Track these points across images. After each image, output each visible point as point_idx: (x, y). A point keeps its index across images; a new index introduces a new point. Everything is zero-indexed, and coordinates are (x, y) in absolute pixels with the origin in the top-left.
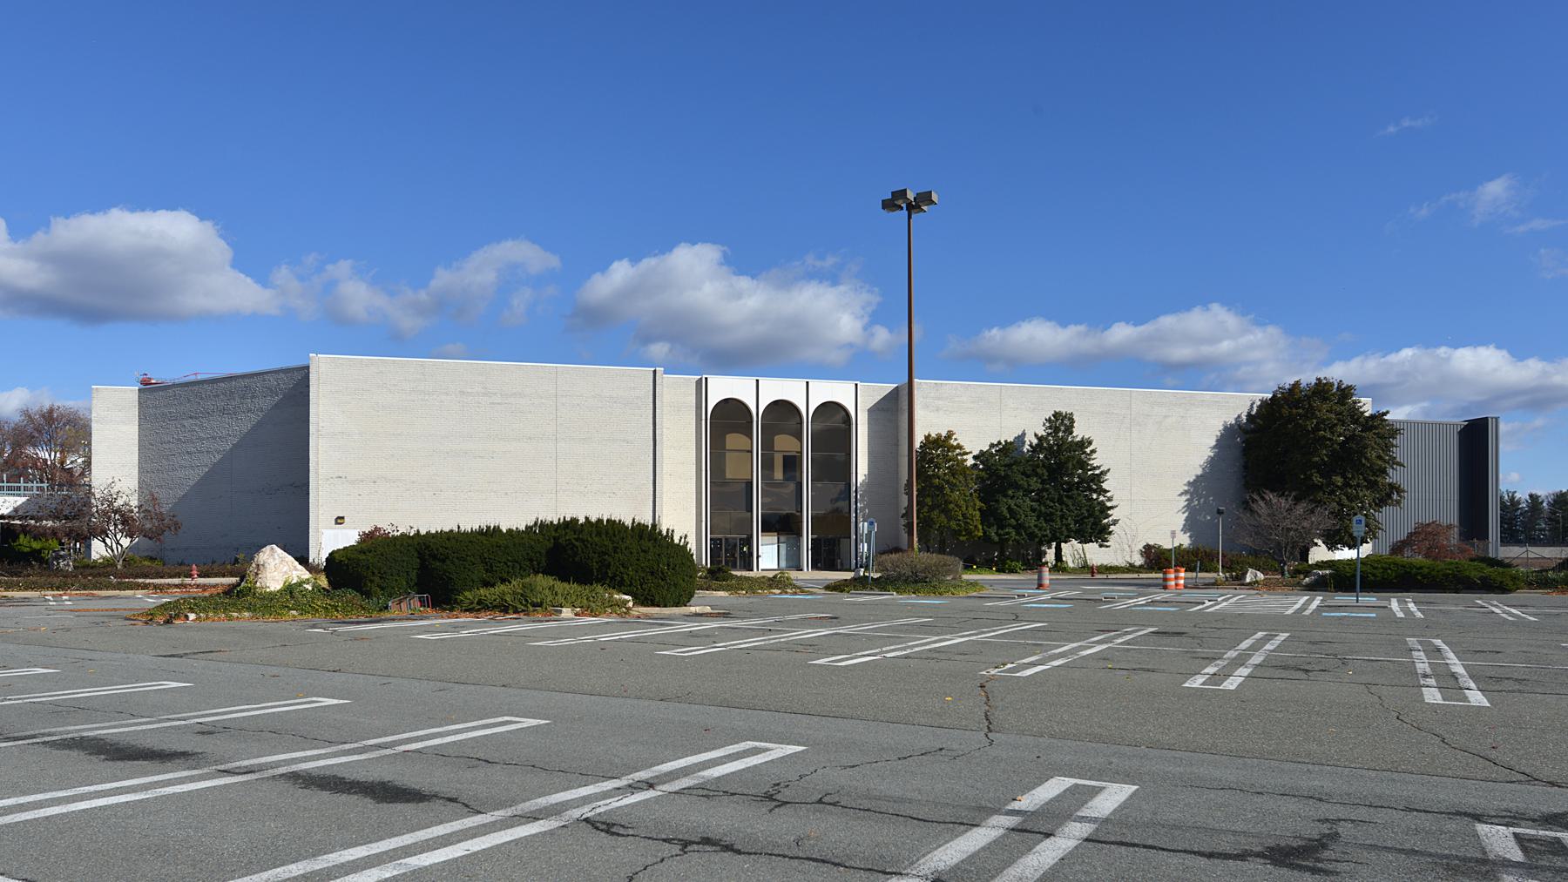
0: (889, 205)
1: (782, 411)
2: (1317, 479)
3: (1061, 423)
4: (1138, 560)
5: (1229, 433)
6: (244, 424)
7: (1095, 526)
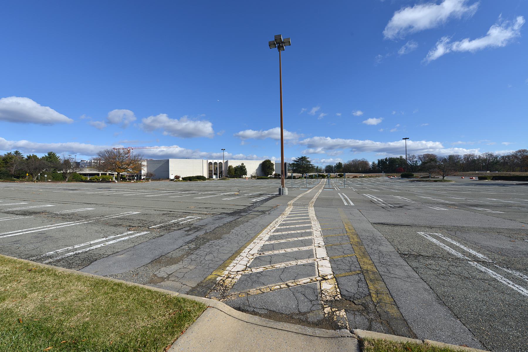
0: (271, 44)
1: (215, 163)
2: (267, 169)
3: (243, 164)
4: (250, 177)
5: (260, 165)
6: (160, 165)
7: (245, 174)
